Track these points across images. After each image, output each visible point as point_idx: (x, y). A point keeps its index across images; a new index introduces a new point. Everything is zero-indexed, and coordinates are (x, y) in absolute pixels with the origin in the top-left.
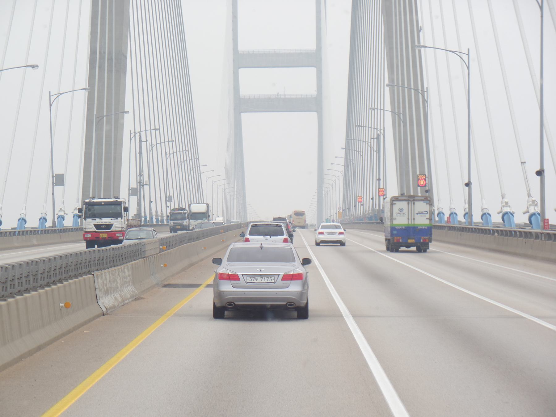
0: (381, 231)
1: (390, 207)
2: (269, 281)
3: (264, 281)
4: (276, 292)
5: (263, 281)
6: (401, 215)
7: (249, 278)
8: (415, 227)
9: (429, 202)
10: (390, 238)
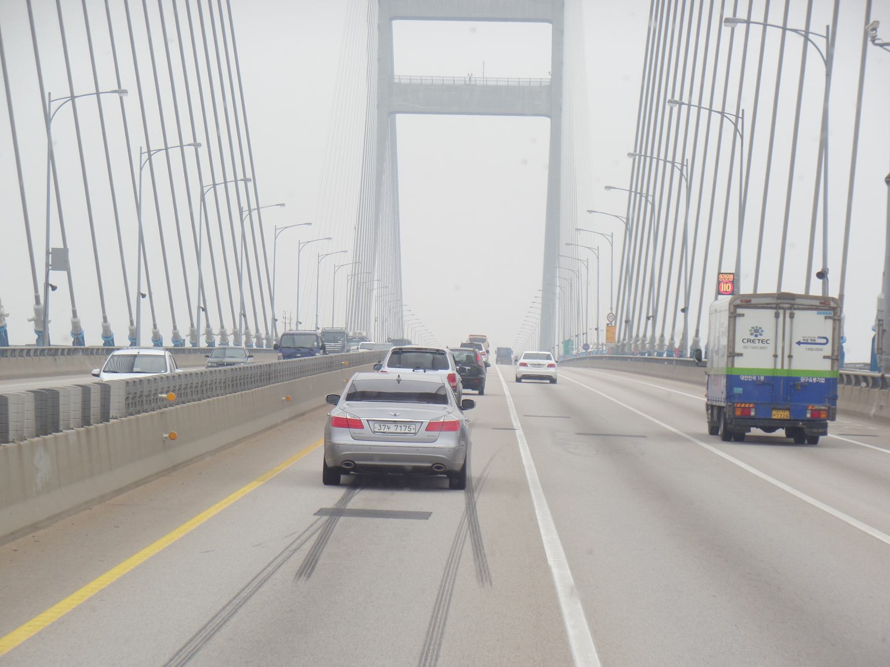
0: (700, 384)
1: (726, 324)
2: (407, 431)
3: (400, 431)
4: (417, 448)
5: (399, 430)
6: (757, 344)
7: (377, 425)
8: (791, 377)
9: (832, 312)
10: (723, 404)
